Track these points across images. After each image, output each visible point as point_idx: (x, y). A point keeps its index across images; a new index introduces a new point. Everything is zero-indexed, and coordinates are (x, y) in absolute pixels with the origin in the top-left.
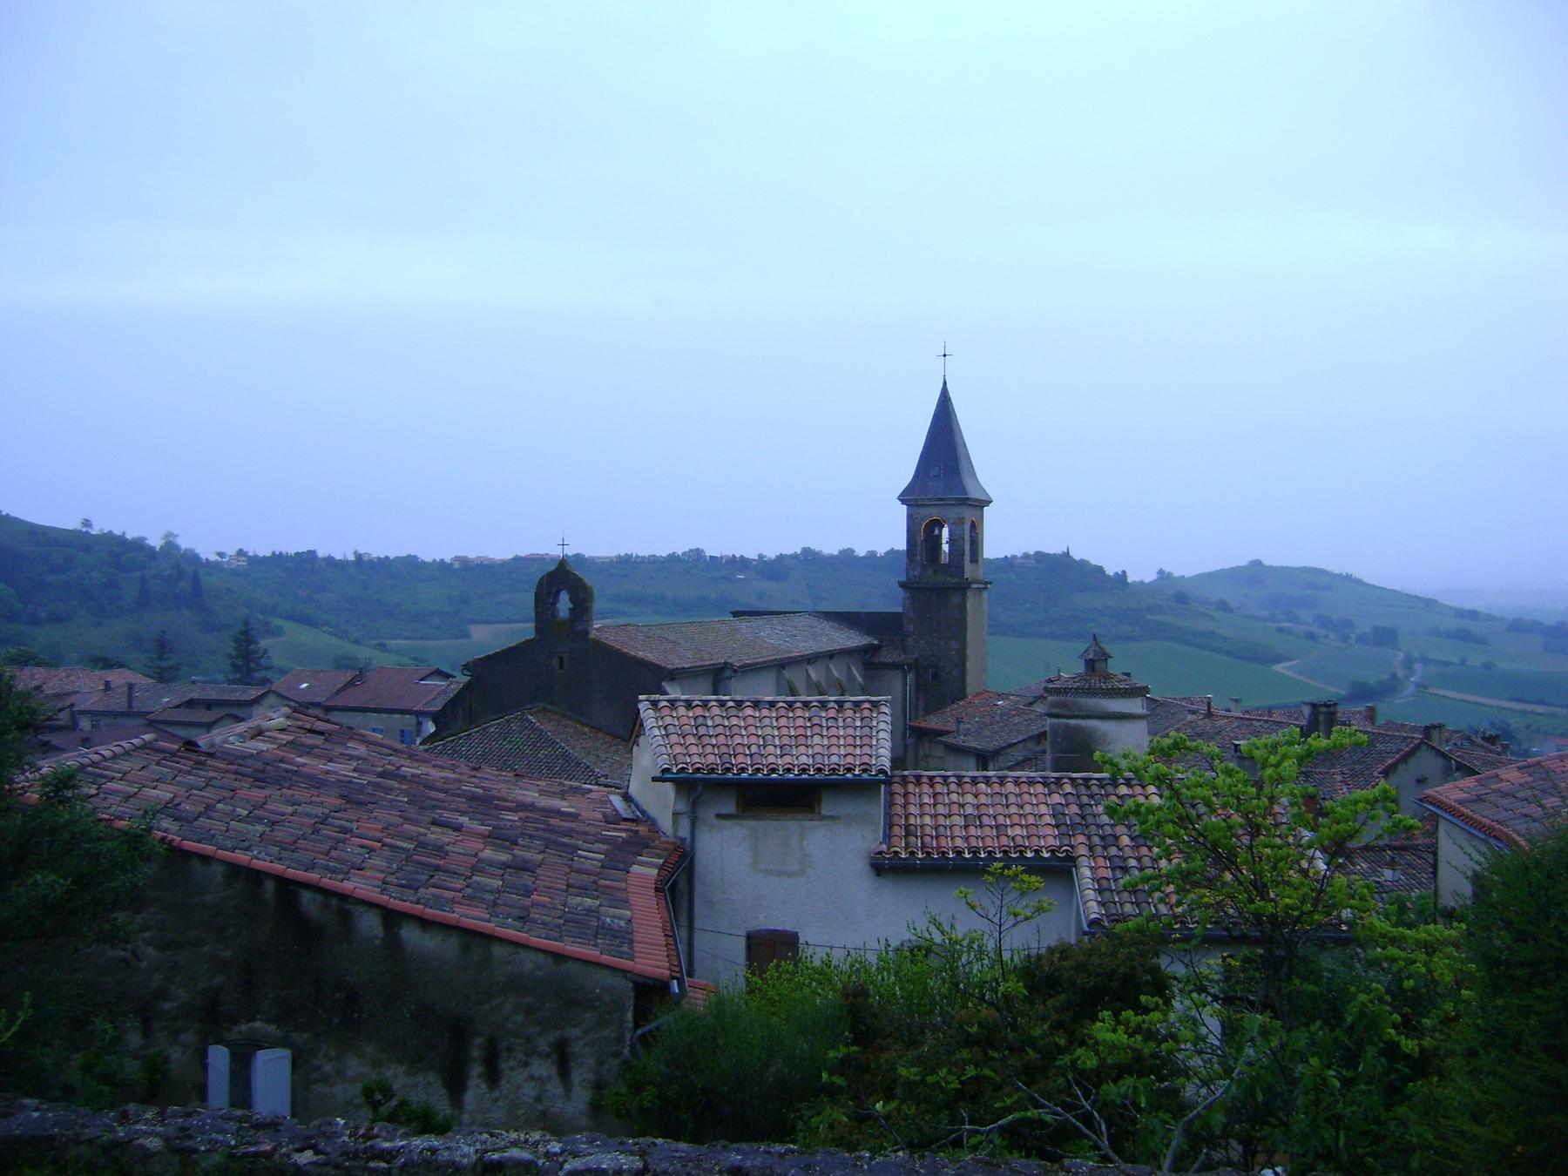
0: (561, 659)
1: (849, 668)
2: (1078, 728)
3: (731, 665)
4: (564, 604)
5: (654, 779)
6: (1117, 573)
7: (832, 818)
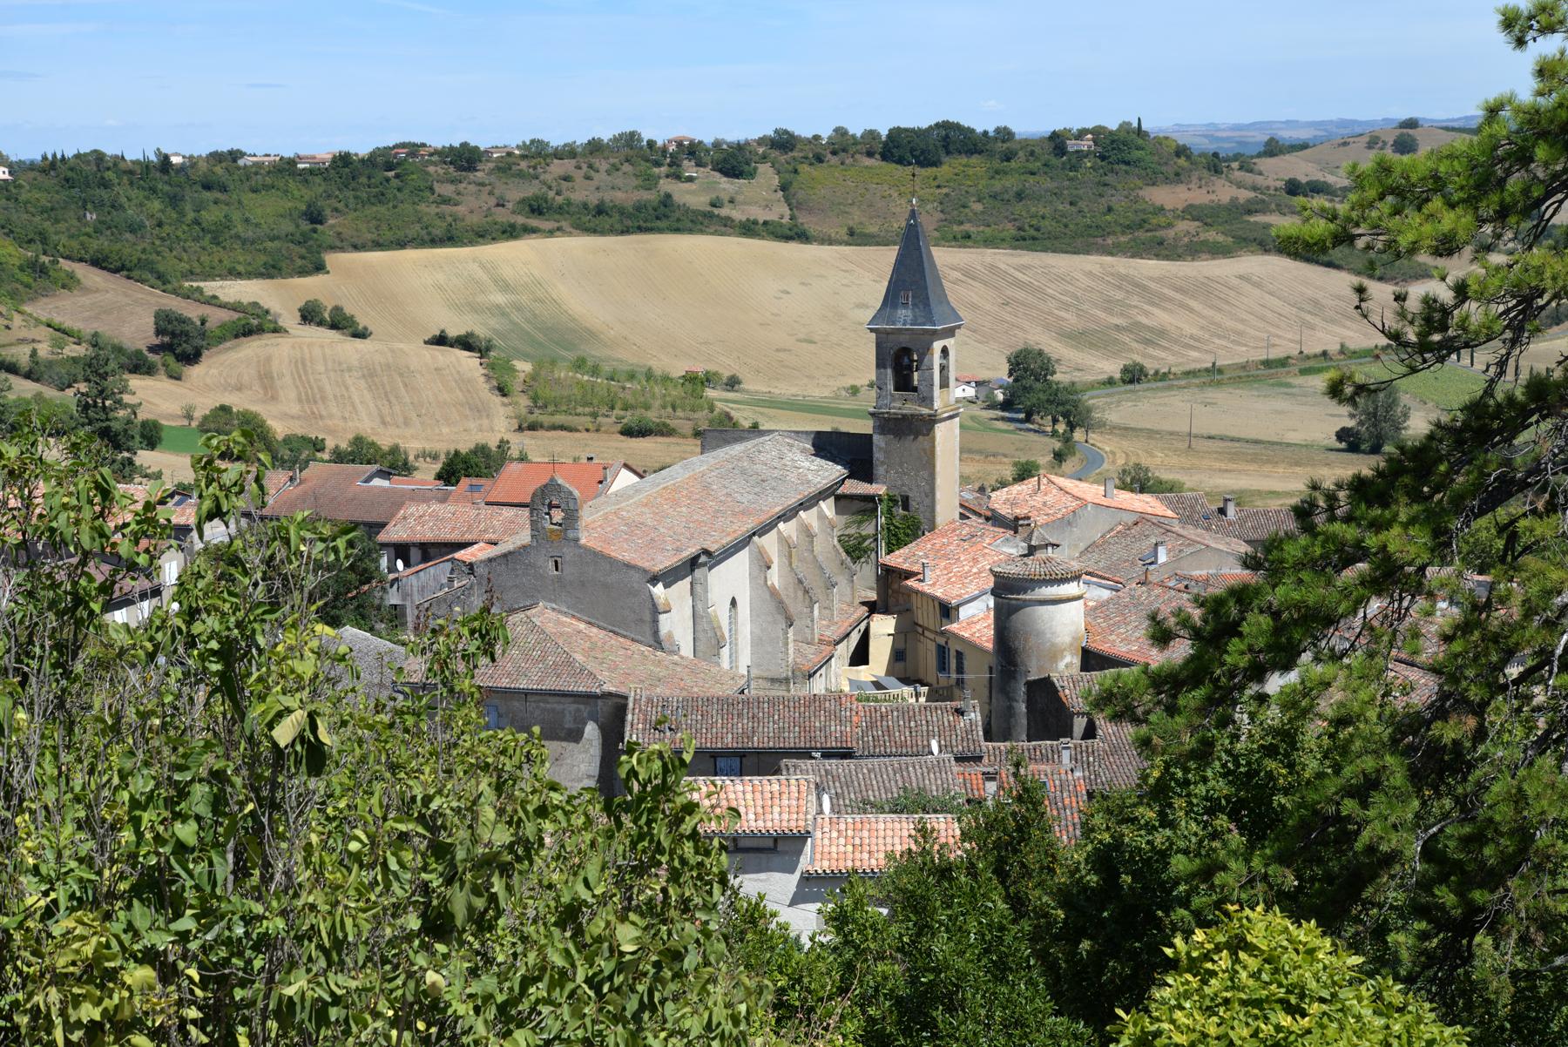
0: (556, 562)
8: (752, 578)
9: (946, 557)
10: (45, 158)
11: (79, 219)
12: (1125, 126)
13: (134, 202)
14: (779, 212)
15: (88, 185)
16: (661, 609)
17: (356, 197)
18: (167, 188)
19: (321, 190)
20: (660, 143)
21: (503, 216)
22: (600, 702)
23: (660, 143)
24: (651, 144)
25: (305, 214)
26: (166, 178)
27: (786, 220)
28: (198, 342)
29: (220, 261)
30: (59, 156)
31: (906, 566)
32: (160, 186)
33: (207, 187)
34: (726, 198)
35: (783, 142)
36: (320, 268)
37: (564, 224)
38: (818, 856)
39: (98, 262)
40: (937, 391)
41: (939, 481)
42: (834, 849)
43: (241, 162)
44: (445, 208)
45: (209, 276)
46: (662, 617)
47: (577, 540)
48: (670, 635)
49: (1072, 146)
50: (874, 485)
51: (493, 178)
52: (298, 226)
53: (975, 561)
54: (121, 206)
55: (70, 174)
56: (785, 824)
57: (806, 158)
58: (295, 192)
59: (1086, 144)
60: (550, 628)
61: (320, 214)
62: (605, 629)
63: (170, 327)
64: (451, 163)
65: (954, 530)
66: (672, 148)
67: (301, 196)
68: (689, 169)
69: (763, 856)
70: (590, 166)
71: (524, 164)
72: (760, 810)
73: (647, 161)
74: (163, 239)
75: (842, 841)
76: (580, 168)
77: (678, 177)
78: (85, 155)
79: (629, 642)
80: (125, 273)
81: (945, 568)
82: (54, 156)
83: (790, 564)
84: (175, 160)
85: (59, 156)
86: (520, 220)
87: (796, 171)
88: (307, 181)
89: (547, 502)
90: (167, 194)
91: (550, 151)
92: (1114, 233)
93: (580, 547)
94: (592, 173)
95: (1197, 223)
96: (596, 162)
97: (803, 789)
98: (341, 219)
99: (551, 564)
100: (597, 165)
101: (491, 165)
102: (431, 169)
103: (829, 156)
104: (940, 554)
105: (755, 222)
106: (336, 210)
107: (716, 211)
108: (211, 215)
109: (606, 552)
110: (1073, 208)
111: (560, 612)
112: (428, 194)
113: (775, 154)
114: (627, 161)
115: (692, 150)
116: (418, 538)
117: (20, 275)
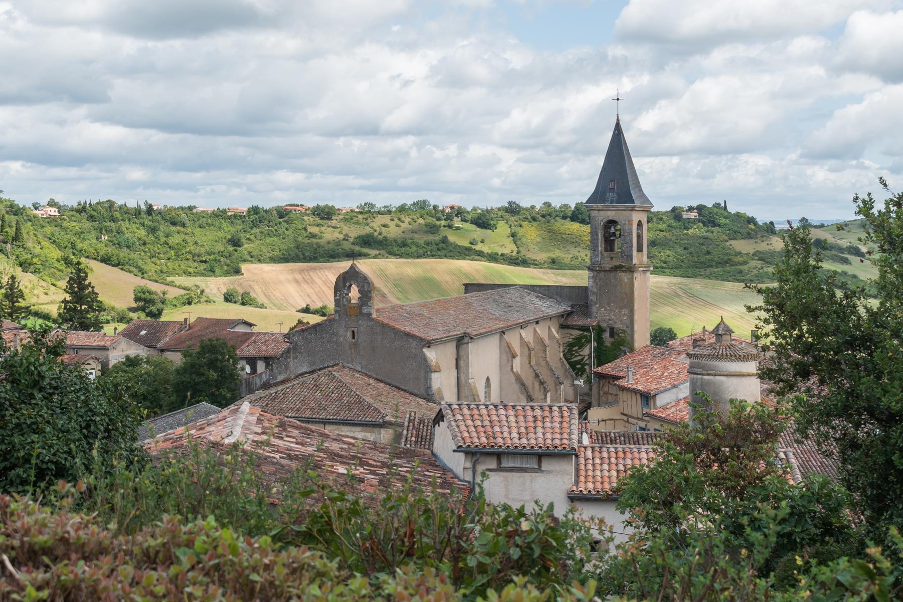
0: (353, 332)
1: (549, 328)
2: (709, 383)
3: (468, 334)
4: (354, 293)
5: (454, 451)
6: (765, 224)
7: (550, 472)
8: (501, 366)
9: (644, 367)
10: (79, 204)
11: (97, 239)
12: (717, 205)
13: (130, 230)
14: (509, 248)
15: (103, 220)
16: (433, 368)
17: (261, 232)
18: (150, 223)
19: (241, 227)
20: (441, 208)
21: (347, 246)
22: (383, 431)
23: (441, 208)
24: (435, 207)
25: (230, 240)
26: (150, 218)
27: (514, 254)
28: (160, 306)
29: (179, 266)
30: (88, 203)
31: (613, 373)
32: (146, 223)
33: (174, 224)
34: (479, 239)
35: (513, 210)
36: (237, 272)
37: (383, 252)
38: (582, 479)
39: (106, 260)
40: (635, 253)
41: (636, 317)
42: (598, 473)
43: (194, 211)
44: (314, 240)
45: (170, 274)
46: (434, 376)
47: (370, 314)
48: (440, 391)
49: (685, 216)
50: (589, 320)
51: (342, 224)
52: (226, 247)
53: (666, 368)
54: (122, 232)
55: (93, 213)
56: (549, 442)
57: (527, 219)
58: (225, 228)
59: (693, 215)
60: (347, 379)
61: (239, 240)
62: (389, 384)
63: (143, 296)
64: (317, 215)
65: (648, 351)
66: (448, 210)
67: (229, 230)
68: (457, 223)
69: (527, 475)
70: (399, 219)
71: (360, 217)
72: (523, 430)
73: (432, 217)
74: (145, 252)
75: (606, 467)
76: (393, 220)
77: (450, 227)
78: (103, 203)
79: (407, 395)
80: (121, 267)
81: (643, 374)
82: (85, 203)
83: (530, 362)
84: (155, 208)
85: (88, 203)
86: (357, 248)
87: (521, 226)
88: (232, 222)
89: (348, 284)
90: (149, 226)
91: (376, 210)
92: (712, 266)
93: (372, 320)
94: (400, 223)
95: (761, 262)
96: (403, 217)
97: (566, 414)
98: (252, 245)
99: (349, 334)
100: (403, 219)
101: (341, 217)
102: (306, 218)
103: (540, 218)
104: (639, 365)
105: (496, 254)
106: (249, 239)
107: (473, 247)
108: (175, 240)
109: (393, 324)
110: (686, 251)
111: (356, 371)
112: (304, 232)
113: (506, 215)
114: (421, 217)
115: (459, 212)
116: (263, 354)
117: (57, 264)
